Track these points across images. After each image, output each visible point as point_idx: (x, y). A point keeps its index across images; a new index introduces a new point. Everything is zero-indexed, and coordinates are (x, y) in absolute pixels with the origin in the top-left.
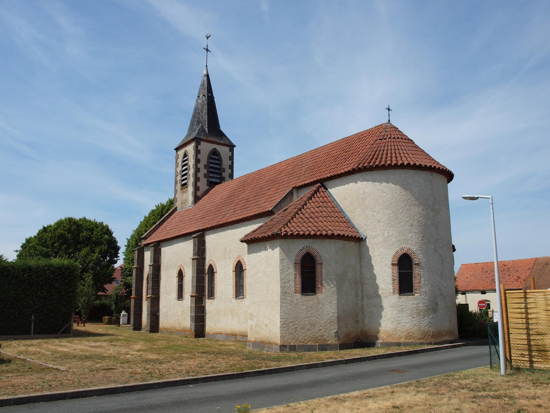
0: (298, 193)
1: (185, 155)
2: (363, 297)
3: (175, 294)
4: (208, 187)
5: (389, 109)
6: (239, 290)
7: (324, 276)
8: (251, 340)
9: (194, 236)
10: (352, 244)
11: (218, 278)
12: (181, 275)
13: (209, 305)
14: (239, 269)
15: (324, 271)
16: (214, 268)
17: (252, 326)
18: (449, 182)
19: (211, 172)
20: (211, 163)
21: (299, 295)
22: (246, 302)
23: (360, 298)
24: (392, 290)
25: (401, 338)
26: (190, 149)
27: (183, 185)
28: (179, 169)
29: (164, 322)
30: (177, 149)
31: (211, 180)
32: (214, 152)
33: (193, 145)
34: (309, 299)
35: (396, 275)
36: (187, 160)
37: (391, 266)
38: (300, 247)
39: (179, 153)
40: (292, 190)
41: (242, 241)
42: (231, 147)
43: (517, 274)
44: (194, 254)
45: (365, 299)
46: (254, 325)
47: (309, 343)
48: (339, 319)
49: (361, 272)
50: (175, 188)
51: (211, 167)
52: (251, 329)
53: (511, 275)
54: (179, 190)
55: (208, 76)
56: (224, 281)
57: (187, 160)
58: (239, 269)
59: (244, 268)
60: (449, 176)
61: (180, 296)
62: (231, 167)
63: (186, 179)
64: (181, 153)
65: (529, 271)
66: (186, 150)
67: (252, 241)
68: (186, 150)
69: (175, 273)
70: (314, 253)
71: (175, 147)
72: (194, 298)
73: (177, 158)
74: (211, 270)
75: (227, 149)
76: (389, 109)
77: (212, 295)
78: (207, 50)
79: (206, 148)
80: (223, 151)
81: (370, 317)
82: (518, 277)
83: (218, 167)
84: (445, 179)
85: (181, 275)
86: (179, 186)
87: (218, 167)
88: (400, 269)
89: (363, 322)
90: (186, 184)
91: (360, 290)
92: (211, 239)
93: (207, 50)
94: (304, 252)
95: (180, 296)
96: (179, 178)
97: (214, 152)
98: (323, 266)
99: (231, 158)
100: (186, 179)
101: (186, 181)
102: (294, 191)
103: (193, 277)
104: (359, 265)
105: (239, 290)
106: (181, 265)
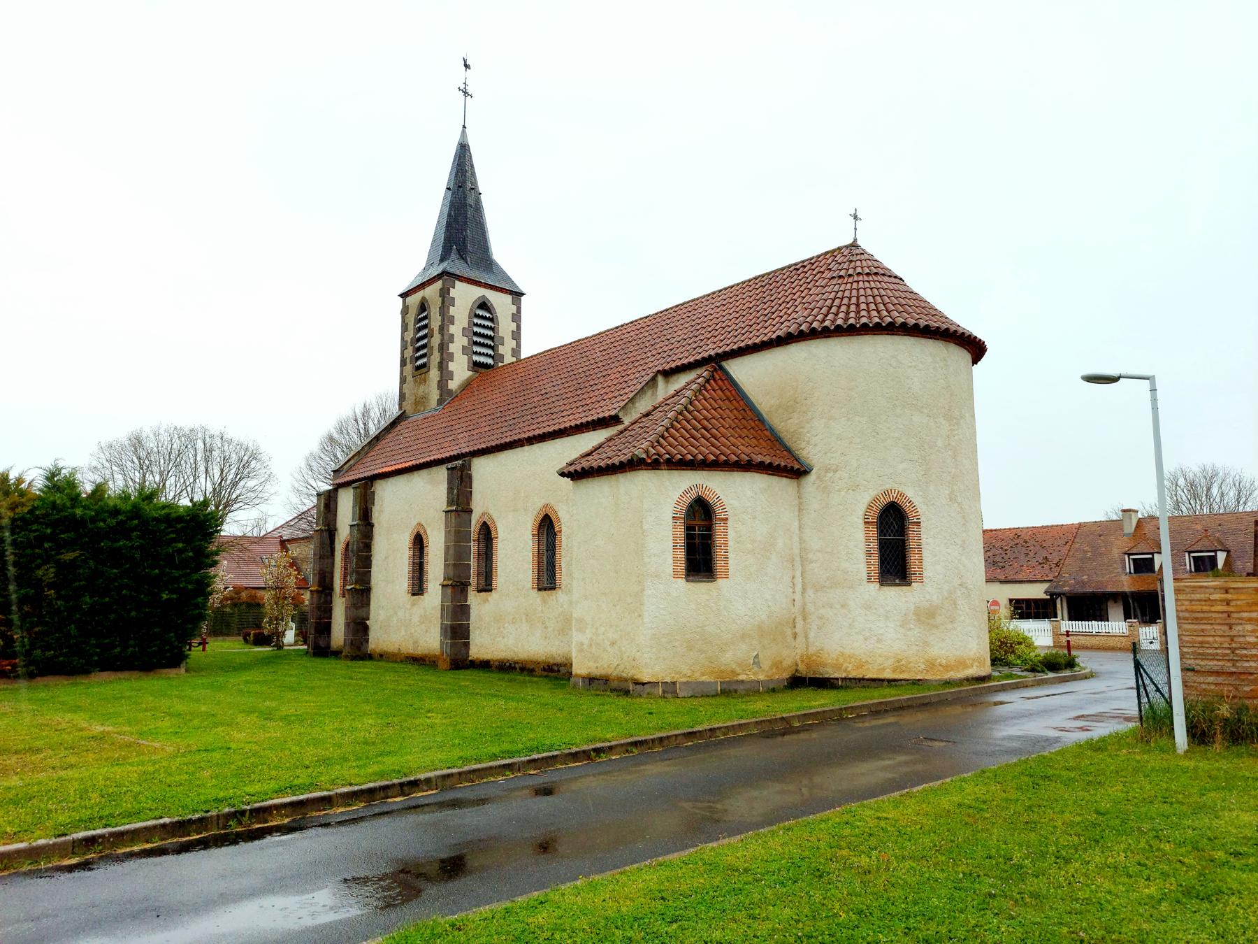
0: (667, 382)
1: (423, 307)
2: (804, 591)
3: (403, 581)
4: (470, 373)
5: (856, 217)
6: (547, 575)
7: (730, 543)
8: (579, 672)
9: (450, 465)
10: (784, 482)
11: (502, 550)
12: (419, 543)
13: (473, 599)
14: (547, 527)
15: (731, 534)
16: (492, 529)
17: (582, 644)
18: (975, 361)
19: (476, 343)
20: (476, 325)
21: (682, 582)
22: (559, 597)
23: (799, 588)
24: (865, 575)
25: (884, 669)
27: (418, 368)
29: (381, 637)
30: (404, 295)
31: (476, 358)
32: (484, 305)
33: (439, 284)
34: (701, 589)
35: (874, 544)
36: (425, 318)
37: (862, 526)
38: (685, 487)
39: (409, 299)
40: (654, 379)
41: (562, 474)
42: (517, 295)
43: (1044, 554)
44: (450, 503)
45: (810, 592)
46: (586, 642)
47: (704, 679)
49: (800, 538)
50: (402, 373)
51: (476, 334)
52: (581, 650)
53: (1032, 554)
54: (409, 378)
55: (463, 152)
56: (515, 554)
57: (425, 318)
58: (547, 527)
59: (557, 529)
60: (976, 349)
61: (418, 587)
62: (516, 335)
63: (424, 356)
64: (414, 300)
65: (1067, 547)
66: (424, 298)
67: (578, 474)
68: (424, 298)
69: (405, 541)
70: (711, 499)
71: (402, 290)
72: (449, 591)
73: (405, 311)
74: (487, 533)
75: (509, 298)
76: (856, 217)
77: (487, 585)
78: (466, 93)
80: (501, 303)
81: (820, 628)
82: (1046, 558)
83: (490, 333)
84: (966, 356)
85: (419, 543)
87: (490, 333)
88: (881, 531)
89: (806, 637)
90: (424, 365)
91: (798, 574)
92: (482, 469)
93: (466, 93)
94: (694, 494)
95: (418, 587)
98: (730, 523)
99: (516, 318)
100: (424, 356)
101: (424, 360)
102: (660, 379)
103: (447, 548)
104: (796, 524)
105: (547, 575)
106: (420, 524)
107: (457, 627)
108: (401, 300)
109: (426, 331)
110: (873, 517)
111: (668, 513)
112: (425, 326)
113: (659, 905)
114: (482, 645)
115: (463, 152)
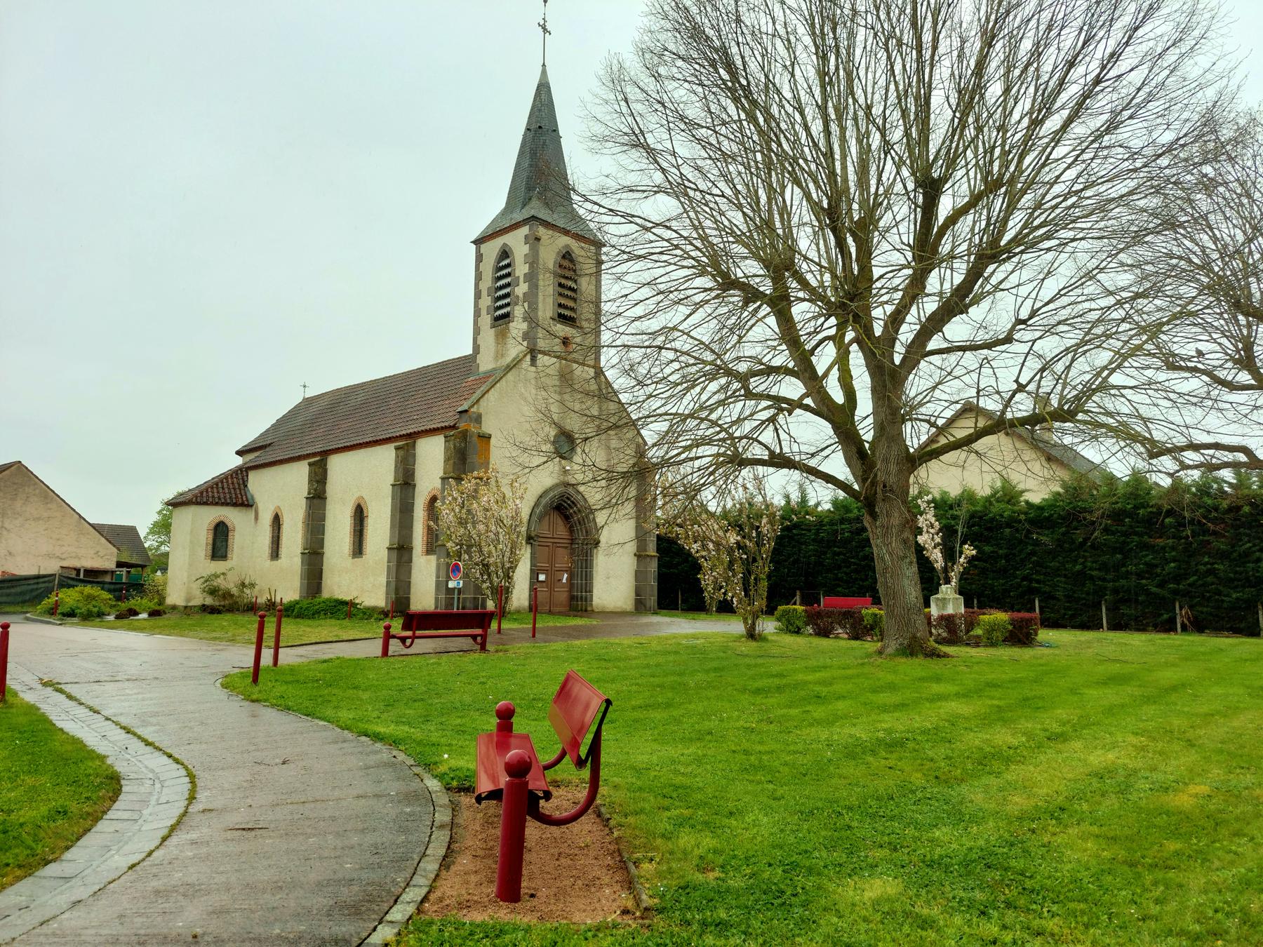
1: (505, 253)
26: (517, 242)
27: (497, 319)
28: (487, 282)
30: (478, 242)
32: (567, 255)
36: (508, 265)
48: (637, 537)
55: (543, 94)
57: (508, 265)
66: (505, 245)
68: (505, 245)
69: (284, 550)
73: (479, 257)
78: (545, 30)
79: (553, 245)
85: (360, 515)
86: (486, 320)
90: (507, 315)
93: (545, 30)
96: (486, 301)
97: (567, 255)
107: (394, 637)
108: (474, 247)
109: (509, 280)
110: (212, 527)
111: (205, 526)
112: (509, 275)
113: (376, 859)
114: (392, 641)
115: (543, 94)
